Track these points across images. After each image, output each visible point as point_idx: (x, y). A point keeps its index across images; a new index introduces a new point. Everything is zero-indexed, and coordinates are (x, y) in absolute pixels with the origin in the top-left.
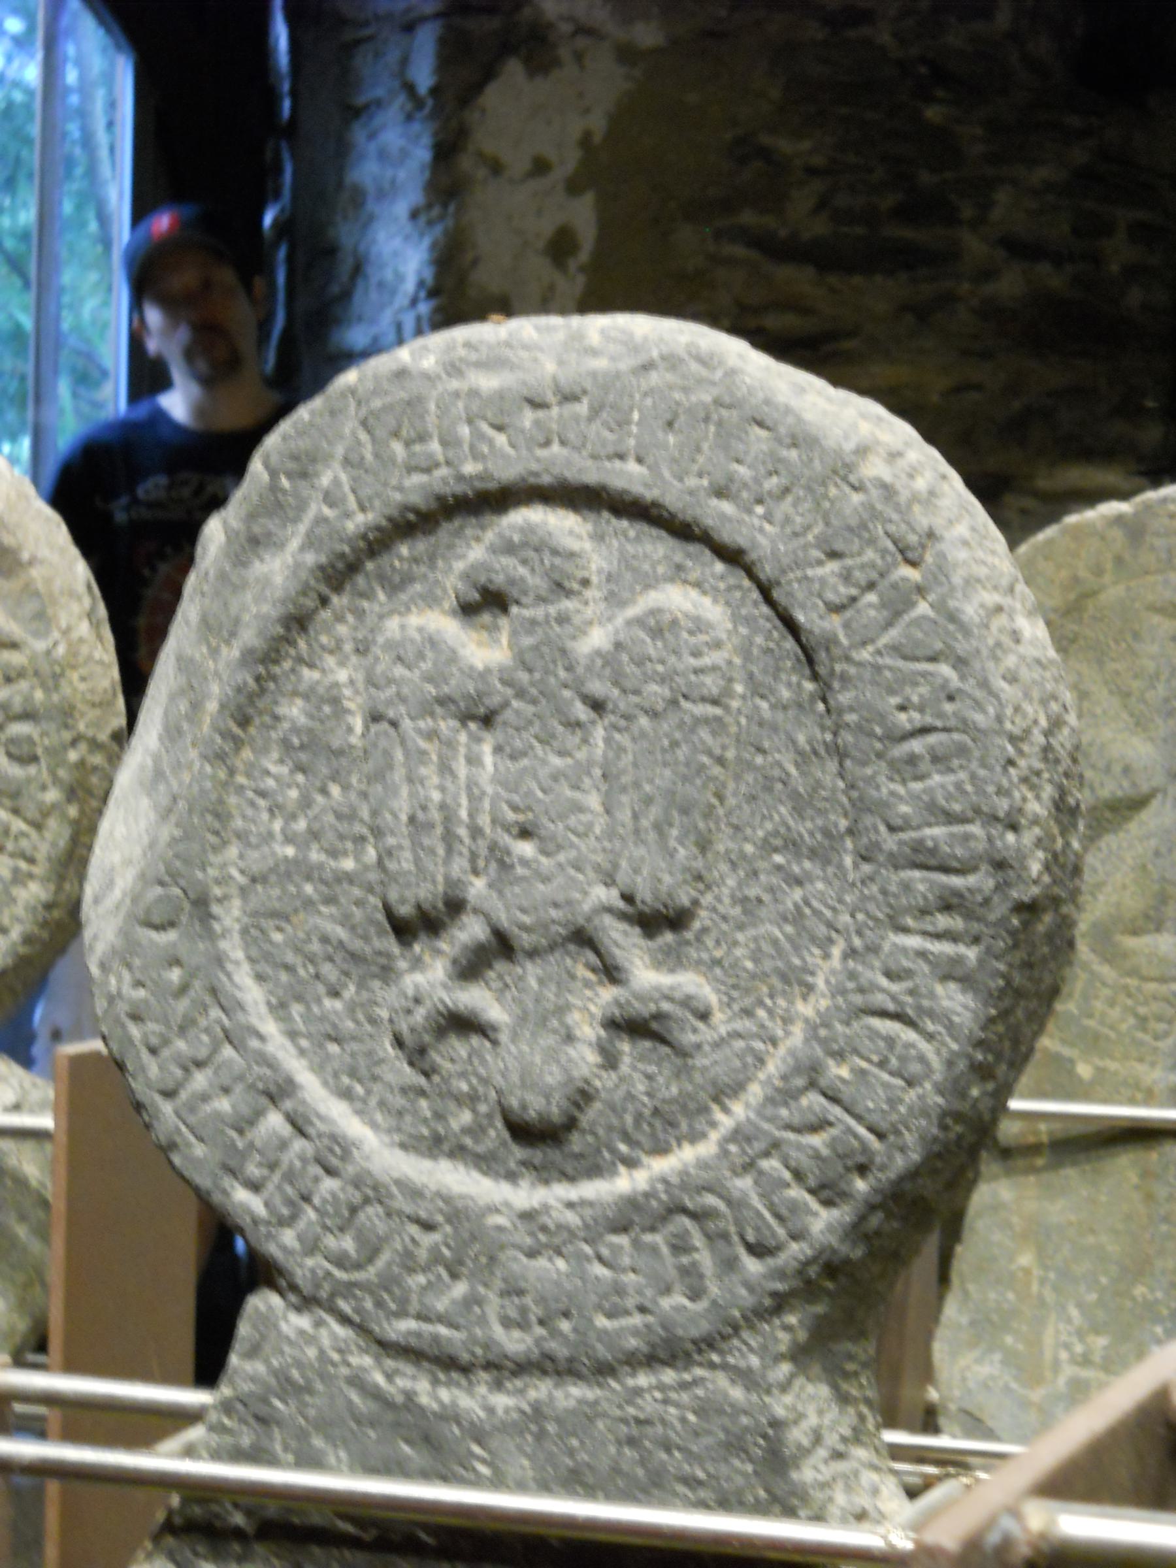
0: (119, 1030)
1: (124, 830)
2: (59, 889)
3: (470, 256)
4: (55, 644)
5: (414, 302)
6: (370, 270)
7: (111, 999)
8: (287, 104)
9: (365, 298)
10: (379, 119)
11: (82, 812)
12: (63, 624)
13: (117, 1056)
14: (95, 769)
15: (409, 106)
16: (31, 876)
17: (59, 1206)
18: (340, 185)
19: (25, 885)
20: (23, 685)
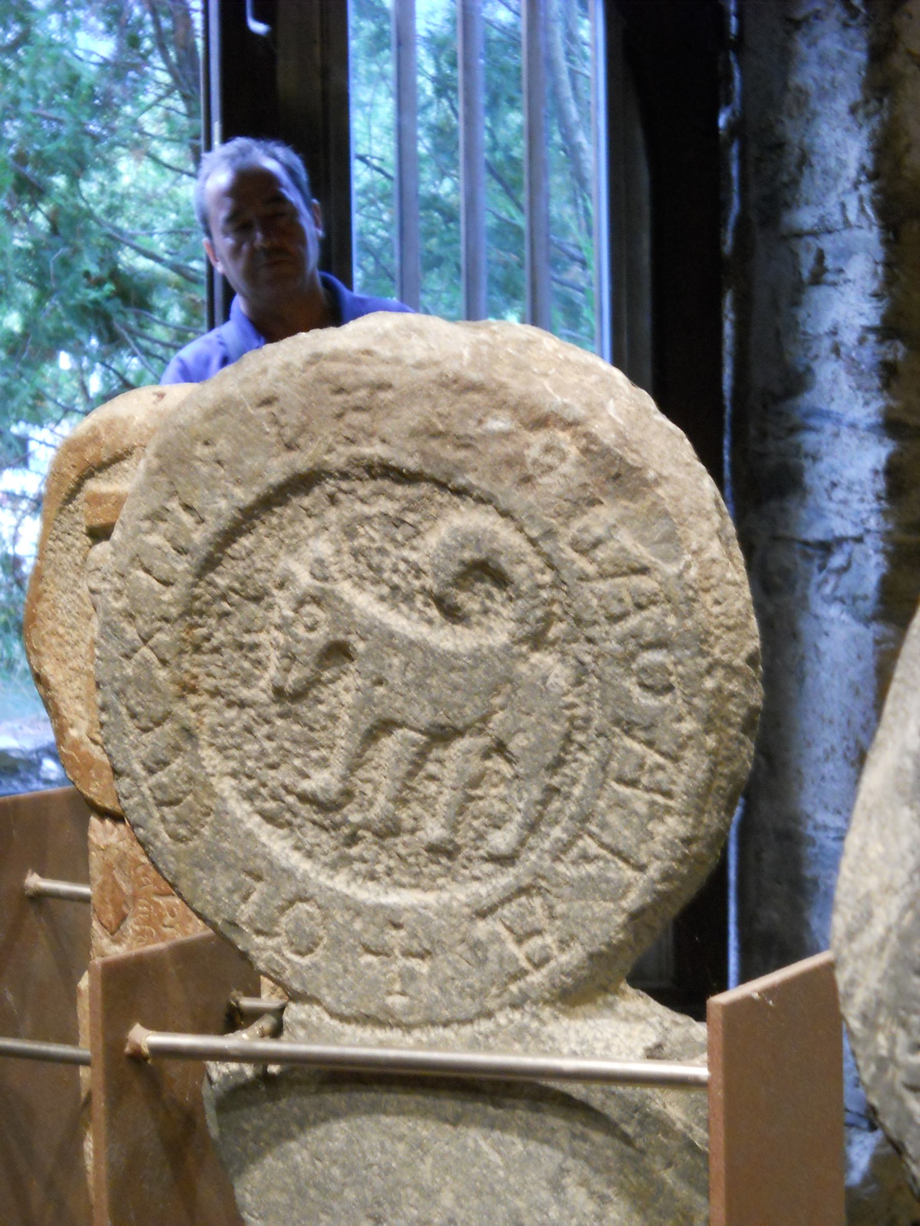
0: (894, 1105)
1: (880, 849)
2: (698, 823)
3: (904, 141)
4: (688, 566)
5: (856, 185)
6: (814, 160)
7: (883, 1063)
8: (734, 21)
9: (811, 184)
10: (819, 28)
11: (720, 741)
12: (694, 546)
13: (894, 1136)
14: (733, 695)
15: (844, 16)
16: (668, 810)
17: (718, 1165)
18: (785, 87)
19: (661, 820)
20: (655, 611)
